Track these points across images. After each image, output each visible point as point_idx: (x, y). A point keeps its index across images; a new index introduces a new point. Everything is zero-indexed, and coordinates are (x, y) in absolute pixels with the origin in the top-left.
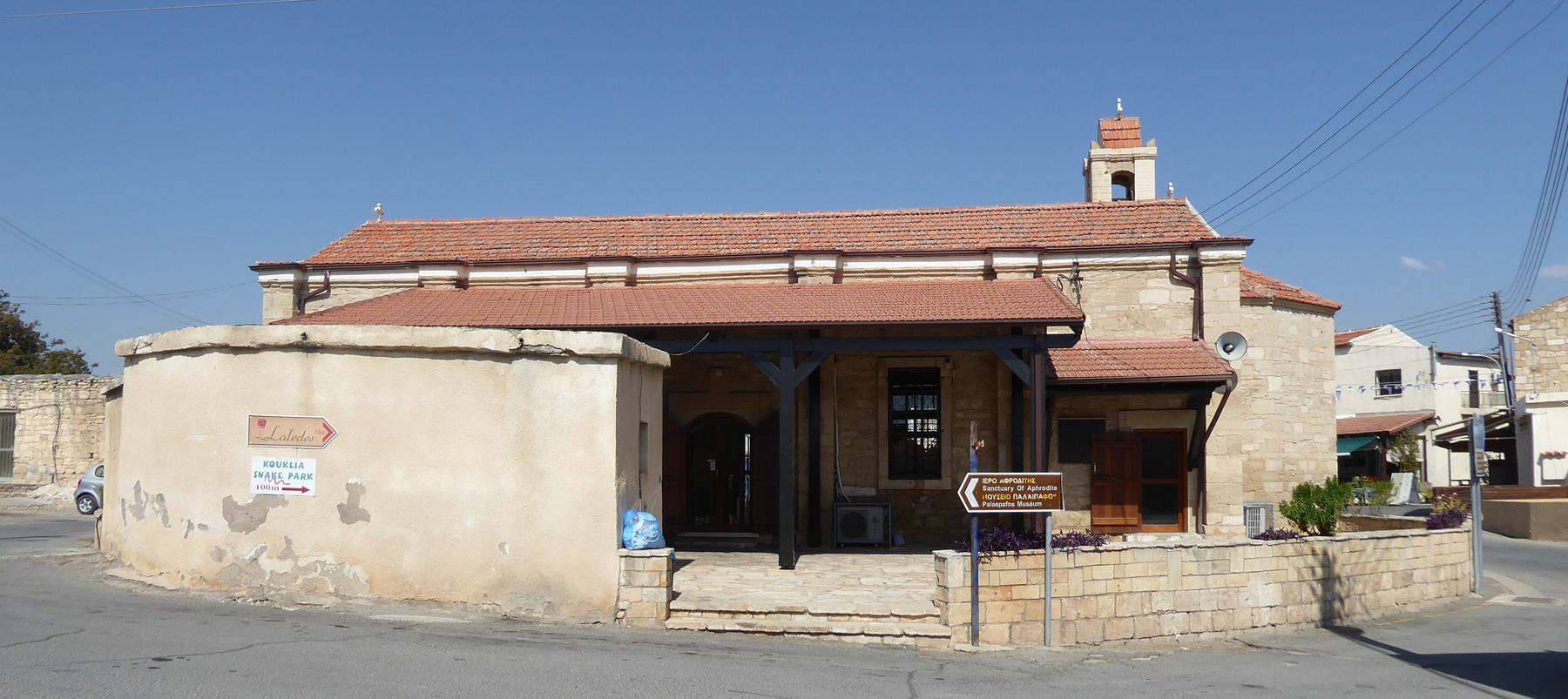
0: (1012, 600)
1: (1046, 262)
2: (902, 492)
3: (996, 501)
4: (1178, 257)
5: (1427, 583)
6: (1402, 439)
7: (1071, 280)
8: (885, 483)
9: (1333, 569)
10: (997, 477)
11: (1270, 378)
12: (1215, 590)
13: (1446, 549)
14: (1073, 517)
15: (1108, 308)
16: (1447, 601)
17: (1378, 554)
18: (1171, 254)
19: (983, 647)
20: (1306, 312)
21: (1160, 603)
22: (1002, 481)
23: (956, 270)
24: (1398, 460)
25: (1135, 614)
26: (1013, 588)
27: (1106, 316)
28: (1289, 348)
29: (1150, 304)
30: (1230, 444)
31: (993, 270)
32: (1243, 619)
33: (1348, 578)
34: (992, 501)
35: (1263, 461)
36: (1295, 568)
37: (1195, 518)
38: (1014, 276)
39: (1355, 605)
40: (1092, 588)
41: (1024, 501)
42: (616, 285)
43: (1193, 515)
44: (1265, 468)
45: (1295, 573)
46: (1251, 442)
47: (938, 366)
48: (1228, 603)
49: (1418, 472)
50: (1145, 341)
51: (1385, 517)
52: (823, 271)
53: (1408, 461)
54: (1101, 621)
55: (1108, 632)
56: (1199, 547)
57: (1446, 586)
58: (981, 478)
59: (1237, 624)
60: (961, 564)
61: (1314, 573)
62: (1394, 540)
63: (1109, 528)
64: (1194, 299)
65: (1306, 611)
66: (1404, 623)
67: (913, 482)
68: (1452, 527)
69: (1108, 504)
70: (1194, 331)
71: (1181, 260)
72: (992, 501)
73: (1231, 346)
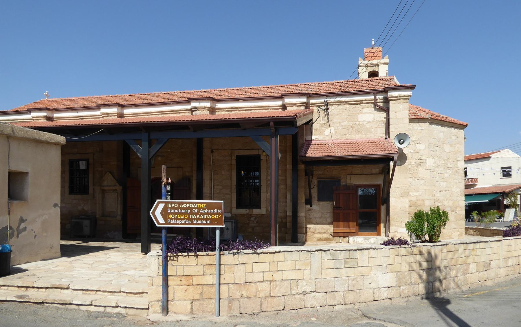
0: (192, 285)
1: (312, 101)
2: (243, 215)
3: (177, 219)
4: (378, 97)
5: (500, 268)
6: (511, 195)
7: (324, 110)
8: (235, 211)
9: (434, 262)
10: (178, 203)
11: (427, 159)
12: (347, 278)
13: (513, 248)
14: (325, 228)
15: (343, 124)
16: (512, 277)
17: (467, 252)
18: (374, 96)
19: (171, 317)
20: (448, 126)
21: (304, 286)
22: (181, 206)
23: (268, 107)
24: (509, 204)
25: (286, 294)
26: (193, 277)
27: (341, 128)
28: (439, 144)
29: (364, 121)
30: (402, 191)
31: (285, 106)
32: (367, 295)
33: (446, 268)
34: (175, 219)
35: (423, 200)
36: (406, 262)
37: (385, 229)
38: (295, 108)
39: (450, 284)
40: (251, 278)
41: (198, 219)
42: (113, 117)
43: (384, 227)
44: (424, 203)
45: (407, 266)
46: (417, 191)
47: (260, 154)
48: (356, 286)
49: (518, 208)
50: (360, 140)
51: (492, 228)
52: (204, 108)
53: (513, 204)
54: (259, 300)
55: (264, 306)
56: (335, 251)
57: (512, 269)
58: (166, 203)
59: (363, 299)
60: (156, 261)
61: (420, 265)
62: (478, 244)
63: (342, 233)
64: (386, 118)
65: (415, 289)
66: (480, 295)
67: (248, 210)
68: (518, 236)
69: (341, 222)
70: (386, 134)
71: (379, 98)
72: (175, 219)
73: (402, 141)
